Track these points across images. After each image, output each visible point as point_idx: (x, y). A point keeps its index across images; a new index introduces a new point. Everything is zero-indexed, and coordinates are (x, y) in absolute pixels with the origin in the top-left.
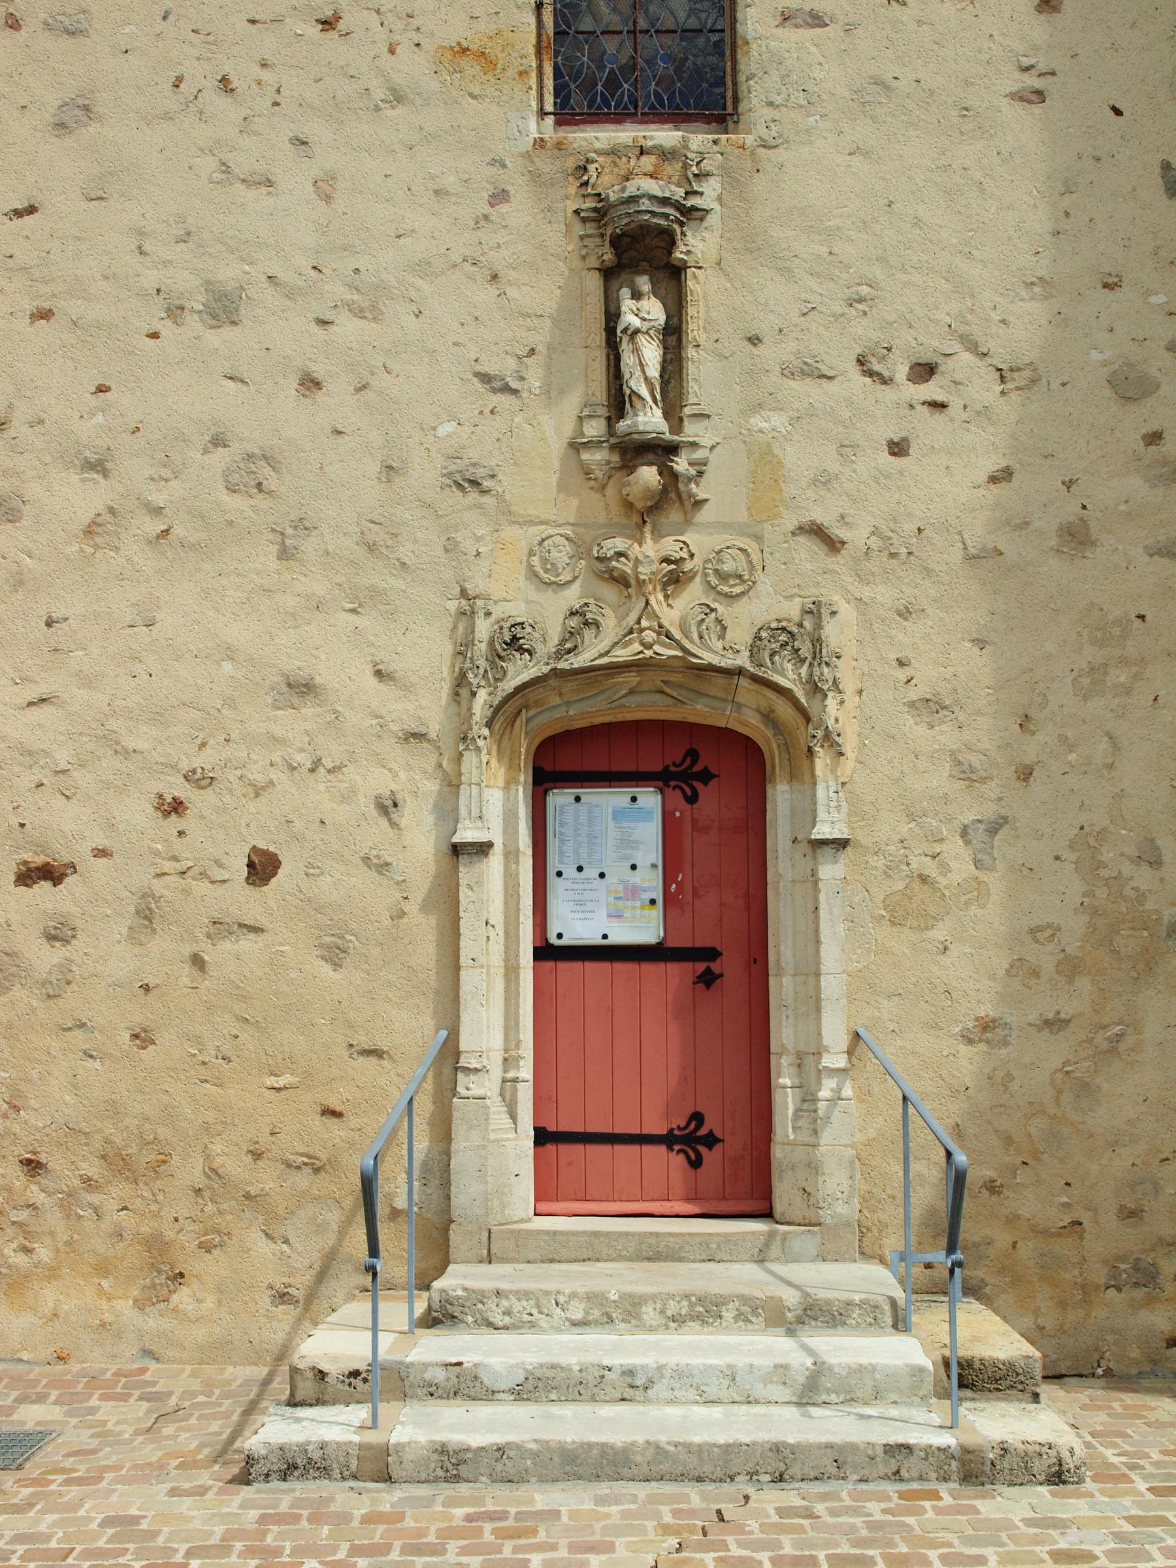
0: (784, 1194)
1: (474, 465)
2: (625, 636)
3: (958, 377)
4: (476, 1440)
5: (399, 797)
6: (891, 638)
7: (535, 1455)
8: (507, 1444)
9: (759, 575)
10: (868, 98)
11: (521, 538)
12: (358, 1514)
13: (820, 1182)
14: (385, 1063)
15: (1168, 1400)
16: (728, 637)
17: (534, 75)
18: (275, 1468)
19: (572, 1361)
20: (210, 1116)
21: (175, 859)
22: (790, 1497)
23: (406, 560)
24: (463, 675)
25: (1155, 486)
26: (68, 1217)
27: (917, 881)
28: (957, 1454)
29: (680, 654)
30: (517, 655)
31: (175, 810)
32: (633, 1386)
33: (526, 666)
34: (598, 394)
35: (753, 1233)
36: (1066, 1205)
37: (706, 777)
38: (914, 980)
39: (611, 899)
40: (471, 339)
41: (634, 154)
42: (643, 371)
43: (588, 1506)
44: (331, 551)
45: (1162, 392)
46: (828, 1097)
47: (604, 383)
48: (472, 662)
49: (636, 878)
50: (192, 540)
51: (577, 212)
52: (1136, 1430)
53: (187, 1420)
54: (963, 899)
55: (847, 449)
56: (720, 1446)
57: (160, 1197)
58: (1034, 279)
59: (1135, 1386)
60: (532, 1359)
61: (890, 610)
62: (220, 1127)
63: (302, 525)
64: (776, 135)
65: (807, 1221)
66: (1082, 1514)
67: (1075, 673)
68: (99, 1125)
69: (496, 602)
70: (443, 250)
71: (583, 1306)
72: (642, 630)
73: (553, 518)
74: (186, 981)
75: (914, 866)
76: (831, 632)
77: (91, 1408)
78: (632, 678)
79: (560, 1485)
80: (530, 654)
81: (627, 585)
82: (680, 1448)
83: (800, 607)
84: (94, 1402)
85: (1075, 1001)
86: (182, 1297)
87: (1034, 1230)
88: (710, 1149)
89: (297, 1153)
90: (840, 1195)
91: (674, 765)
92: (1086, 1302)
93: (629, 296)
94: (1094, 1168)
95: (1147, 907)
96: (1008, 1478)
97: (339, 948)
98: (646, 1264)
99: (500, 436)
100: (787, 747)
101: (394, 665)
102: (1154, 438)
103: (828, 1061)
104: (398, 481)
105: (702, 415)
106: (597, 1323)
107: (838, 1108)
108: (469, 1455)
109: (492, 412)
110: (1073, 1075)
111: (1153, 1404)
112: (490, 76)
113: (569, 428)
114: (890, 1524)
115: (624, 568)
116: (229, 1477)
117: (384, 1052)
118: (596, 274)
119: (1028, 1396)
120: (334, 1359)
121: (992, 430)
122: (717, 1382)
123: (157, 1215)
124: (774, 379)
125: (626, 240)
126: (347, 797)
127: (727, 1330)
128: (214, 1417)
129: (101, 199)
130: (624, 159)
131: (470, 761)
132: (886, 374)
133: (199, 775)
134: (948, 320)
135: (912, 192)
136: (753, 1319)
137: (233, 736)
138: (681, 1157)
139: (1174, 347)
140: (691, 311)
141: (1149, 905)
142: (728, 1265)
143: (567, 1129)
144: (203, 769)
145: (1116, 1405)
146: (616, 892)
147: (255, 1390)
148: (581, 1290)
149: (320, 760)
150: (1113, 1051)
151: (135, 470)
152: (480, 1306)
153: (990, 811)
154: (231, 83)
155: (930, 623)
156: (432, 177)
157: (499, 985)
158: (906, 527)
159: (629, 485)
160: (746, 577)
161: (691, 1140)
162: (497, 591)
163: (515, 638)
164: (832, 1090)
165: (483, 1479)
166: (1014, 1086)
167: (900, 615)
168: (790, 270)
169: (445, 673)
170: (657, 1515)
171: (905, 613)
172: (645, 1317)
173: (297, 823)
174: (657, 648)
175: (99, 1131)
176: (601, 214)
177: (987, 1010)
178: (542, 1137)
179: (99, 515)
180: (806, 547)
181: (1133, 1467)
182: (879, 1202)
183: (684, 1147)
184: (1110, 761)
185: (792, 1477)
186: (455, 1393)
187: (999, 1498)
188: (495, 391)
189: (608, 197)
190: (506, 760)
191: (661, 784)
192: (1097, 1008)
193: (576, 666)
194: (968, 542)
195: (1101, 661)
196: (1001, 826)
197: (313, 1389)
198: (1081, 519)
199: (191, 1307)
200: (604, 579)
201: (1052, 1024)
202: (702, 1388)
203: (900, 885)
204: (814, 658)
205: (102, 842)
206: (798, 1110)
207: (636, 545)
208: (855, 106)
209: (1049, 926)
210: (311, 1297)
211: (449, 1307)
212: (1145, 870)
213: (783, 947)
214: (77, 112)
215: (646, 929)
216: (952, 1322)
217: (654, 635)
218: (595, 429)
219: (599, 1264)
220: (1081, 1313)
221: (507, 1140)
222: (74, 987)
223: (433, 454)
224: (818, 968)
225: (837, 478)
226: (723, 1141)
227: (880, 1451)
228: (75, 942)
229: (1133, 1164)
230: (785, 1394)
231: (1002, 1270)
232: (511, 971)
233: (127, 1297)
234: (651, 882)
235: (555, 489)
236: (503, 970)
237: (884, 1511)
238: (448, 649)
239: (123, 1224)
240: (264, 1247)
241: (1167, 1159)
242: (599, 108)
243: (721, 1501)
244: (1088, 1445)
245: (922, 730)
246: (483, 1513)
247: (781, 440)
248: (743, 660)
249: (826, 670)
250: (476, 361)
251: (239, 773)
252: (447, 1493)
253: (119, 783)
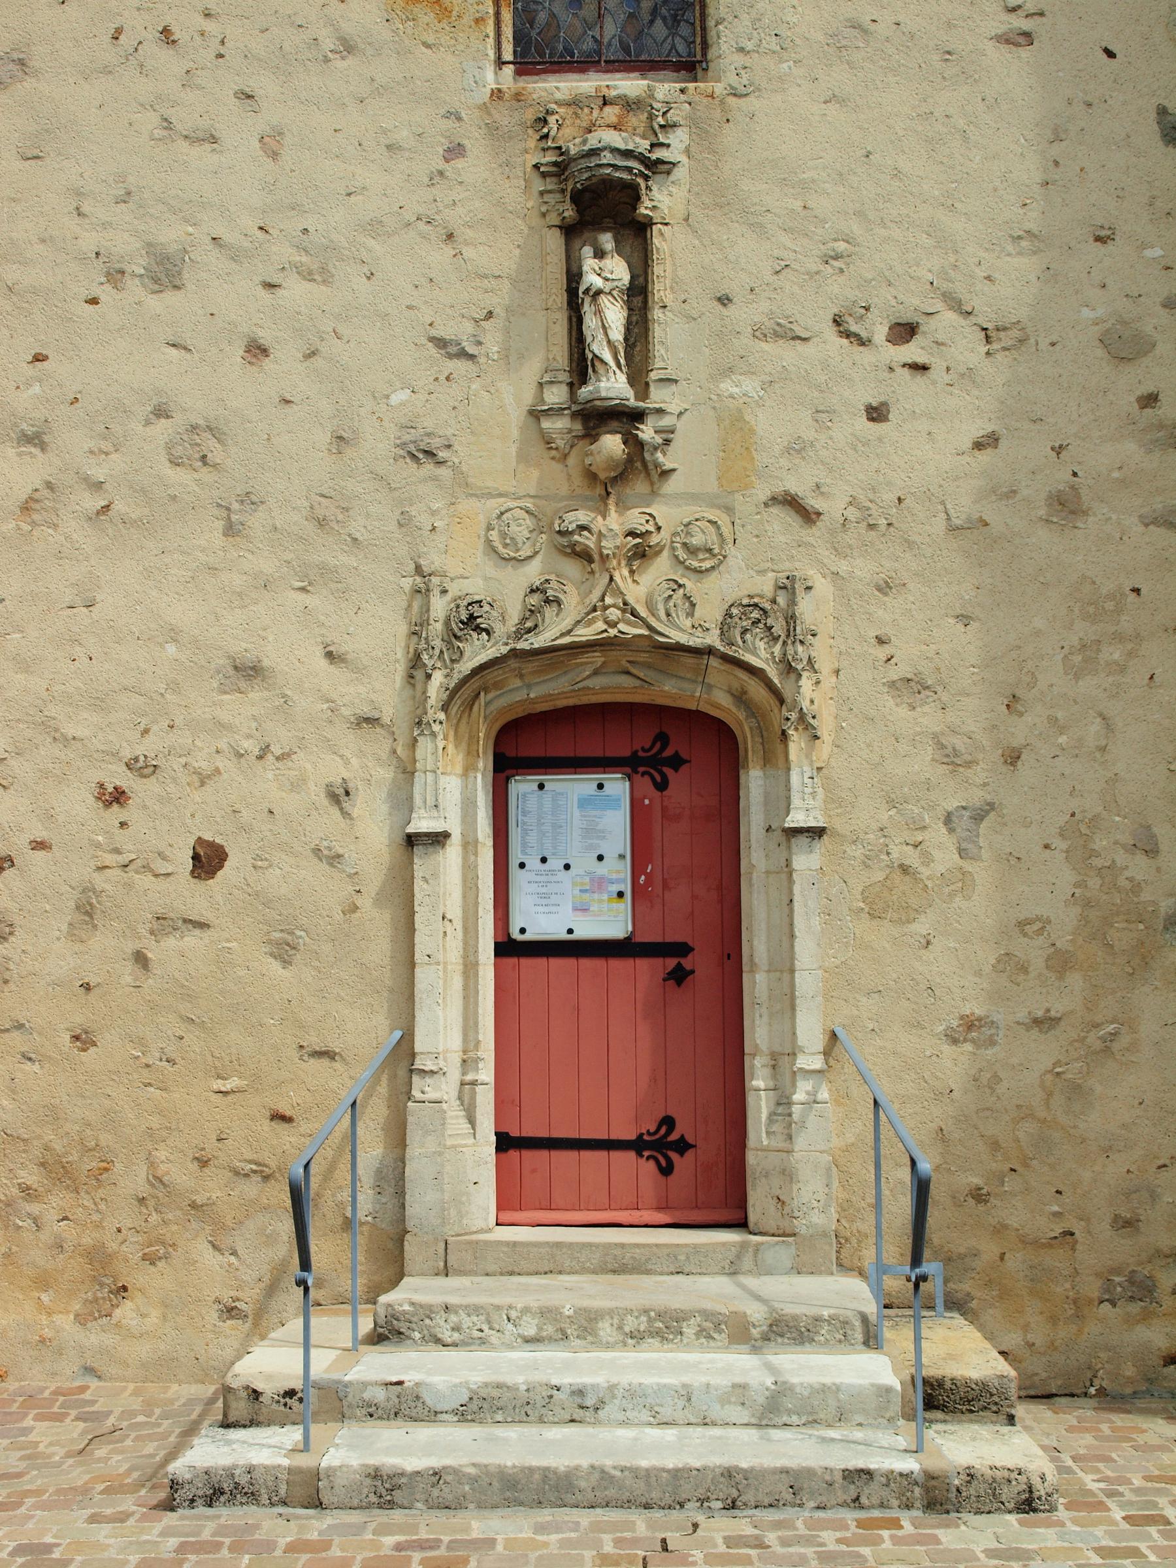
0: (758, 1204)
1: (428, 435)
2: (588, 614)
3: (940, 337)
4: (412, 1464)
5: (351, 785)
6: (870, 614)
7: (474, 1480)
8: (444, 1468)
9: (730, 549)
10: (844, 43)
11: (482, 510)
12: (282, 1542)
13: (795, 1190)
14: (337, 1065)
15: (1161, 1421)
16: (697, 614)
17: (491, 22)
18: (200, 1493)
19: (519, 1380)
20: (155, 1122)
21: (117, 851)
22: (741, 1525)
23: (358, 535)
24: (418, 656)
25: (1150, 451)
26: (6, 1227)
27: (898, 872)
28: (921, 1480)
29: (646, 633)
30: (475, 635)
31: (117, 800)
32: (584, 1407)
33: (484, 647)
34: (559, 358)
35: (724, 1244)
36: (1056, 1214)
37: (677, 762)
38: (895, 976)
39: (577, 892)
40: (426, 302)
41: (596, 108)
42: (606, 334)
43: (527, 1534)
44: (279, 526)
45: (1159, 349)
46: (803, 1100)
47: (566, 346)
48: (427, 643)
49: (602, 869)
50: (133, 516)
51: (536, 167)
52: (1122, 1454)
53: (122, 1441)
54: (947, 890)
55: (822, 415)
56: (668, 1471)
57: (102, 1206)
58: (1021, 233)
59: (1128, 1407)
60: (477, 1378)
61: (868, 584)
62: (164, 1133)
63: (249, 500)
64: (746, 83)
65: (781, 1232)
66: (1049, 1544)
67: (1066, 651)
68: (38, 1131)
69: (452, 579)
70: (396, 209)
71: (536, 1321)
72: (606, 608)
73: (513, 490)
74: (128, 979)
75: (895, 855)
76: (806, 607)
77: (25, 1429)
78: (597, 658)
79: (500, 1512)
80: (488, 633)
81: (590, 560)
82: (627, 1473)
83: (772, 582)
84: (29, 1422)
85: (1066, 997)
86: (126, 1312)
87: (1024, 1241)
88: (682, 1155)
89: (246, 1161)
90: (815, 1204)
91: (643, 750)
92: (1079, 1316)
93: (592, 254)
94: (1087, 1175)
95: (1142, 899)
96: (974, 1505)
97: (288, 945)
98: (611, 1277)
99: (456, 404)
100: (762, 730)
101: (344, 646)
102: (1150, 400)
103: (802, 1062)
104: (349, 452)
105: (669, 380)
106: (550, 1339)
107: (814, 1112)
108: (404, 1480)
109: (448, 379)
110: (1063, 1076)
111: (1145, 1426)
112: (444, 24)
113: (528, 397)
114: (842, 1554)
115: (587, 542)
116: (155, 1502)
117: (336, 1054)
118: (557, 232)
119: (1003, 1417)
120: (269, 1377)
121: (976, 392)
122: (671, 1403)
123: (99, 1226)
124: (746, 341)
125: (587, 195)
126: (297, 786)
127: (688, 1348)
128: (150, 1438)
129: (37, 157)
130: (586, 110)
131: (425, 746)
132: (864, 334)
133: (141, 763)
134: (930, 277)
135: (892, 142)
136: (716, 1335)
137: (177, 722)
138: (652, 1163)
139: (1173, 304)
140: (657, 270)
141: (1146, 896)
142: (697, 1278)
143: (531, 1134)
144: (145, 756)
145: (1105, 1427)
146: (582, 884)
147: (198, 1409)
148: (534, 1305)
149: (268, 746)
150: (1107, 1050)
151: (74, 442)
152: (427, 1321)
153: (977, 797)
154: (173, 34)
155: (912, 599)
156: (385, 132)
157: (457, 982)
158: (885, 497)
159: (592, 454)
160: (716, 551)
161: (661, 1145)
162: (453, 568)
163: (472, 617)
164: (808, 1093)
165: (419, 1505)
166: (1001, 1089)
167: (879, 589)
168: (761, 226)
169: (400, 654)
170: (598, 1544)
171: (884, 588)
172: (601, 1333)
173: (244, 813)
174: (621, 626)
175: (39, 1137)
176: (561, 168)
177: (977, 1009)
178: (505, 1143)
179: (36, 490)
180: (781, 517)
181: (1111, 1494)
182: (859, 1211)
183: (655, 1154)
184: (1104, 743)
185: (745, 1504)
186: (396, 1414)
187: (963, 1528)
188: (450, 356)
189: (568, 150)
190: (464, 745)
191: (628, 770)
192: (1089, 1005)
193: (536, 646)
194: (952, 512)
195: (1093, 638)
196: (987, 812)
197: (245, 1409)
198: (1072, 487)
199: (135, 1322)
200: (566, 554)
201: (1042, 1022)
202: (656, 1409)
203: (879, 876)
204: (788, 636)
205: (41, 834)
206: (772, 1114)
207: (600, 518)
208: (831, 50)
209: (1039, 918)
210: (260, 1313)
211: (395, 1322)
212: (1140, 859)
213: (757, 944)
214: (11, 66)
215: (611, 922)
216: (918, 1340)
217: (619, 613)
218: (556, 395)
219: (561, 1277)
220: (1073, 1328)
221: (466, 1146)
222: (12, 986)
223: (386, 423)
224: (793, 964)
225: (812, 445)
226: (695, 1146)
227: (838, 1477)
228: (12, 939)
229: (1128, 1171)
230: (744, 1416)
231: (989, 1283)
232: (470, 968)
233: (68, 1312)
234: (619, 872)
235: (514, 460)
236: (461, 967)
237: (839, 1541)
238: (403, 629)
239: (64, 1235)
240: (210, 1259)
241: (1165, 1166)
242: (562, 56)
243: (667, 1530)
244: (1062, 1470)
245: (903, 711)
246: (414, 1541)
247: (753, 405)
248: (712, 639)
249: (800, 648)
250: (431, 325)
251: (183, 760)
252: (380, 1520)
253: (58, 772)
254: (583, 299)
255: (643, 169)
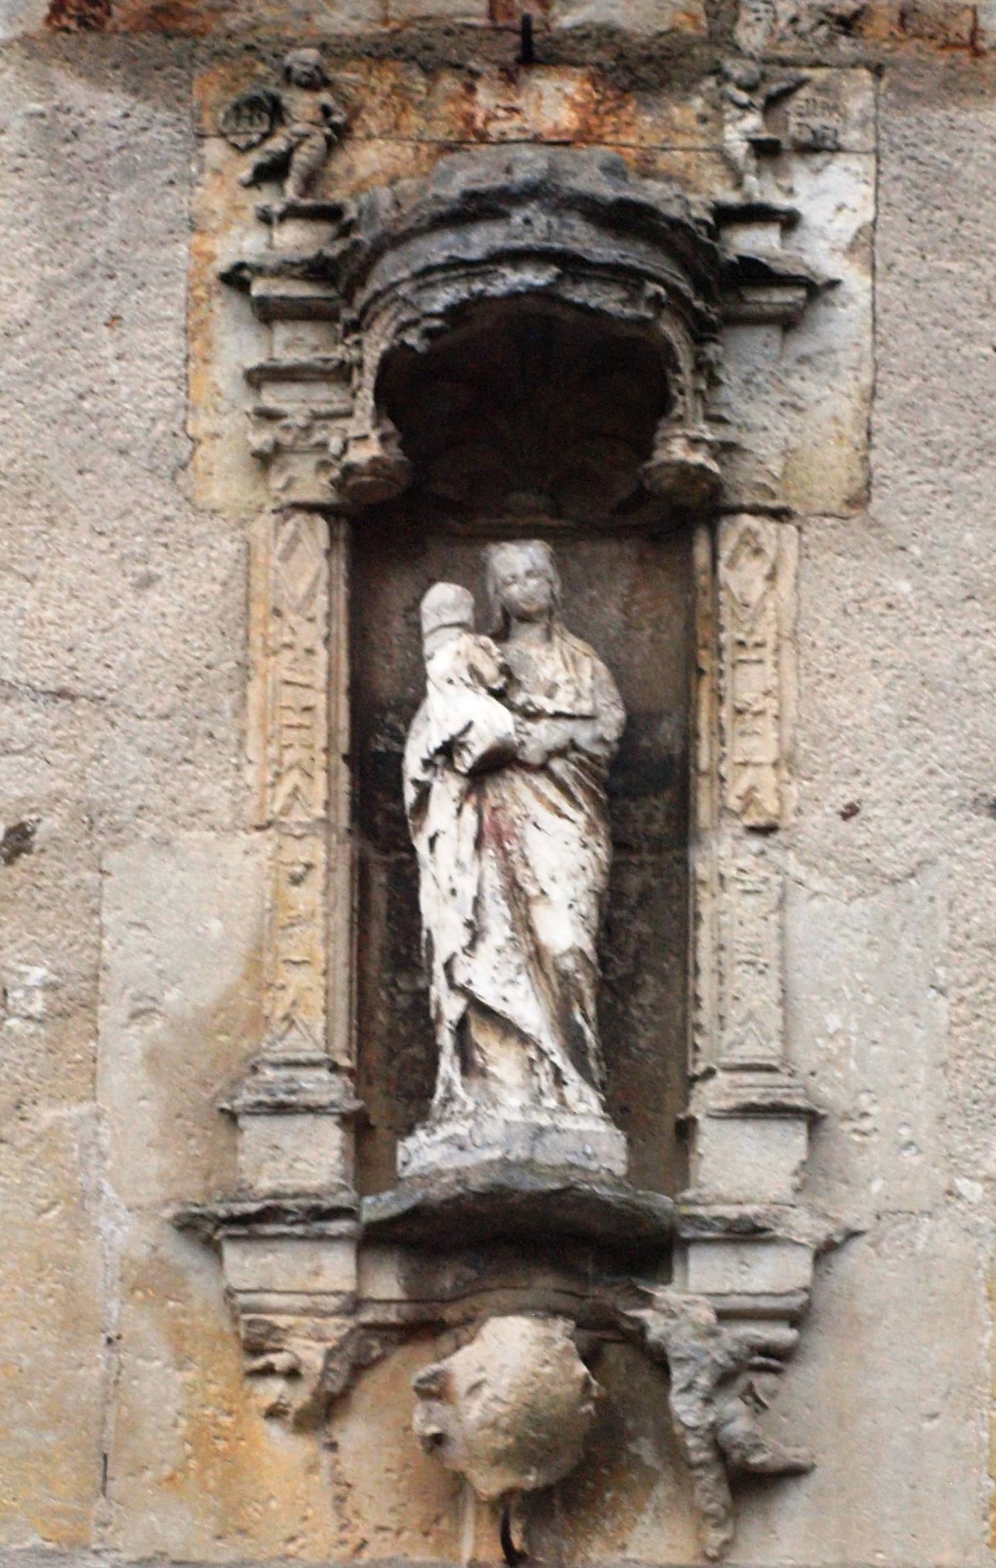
254: (424, 790)
255: (685, 287)
